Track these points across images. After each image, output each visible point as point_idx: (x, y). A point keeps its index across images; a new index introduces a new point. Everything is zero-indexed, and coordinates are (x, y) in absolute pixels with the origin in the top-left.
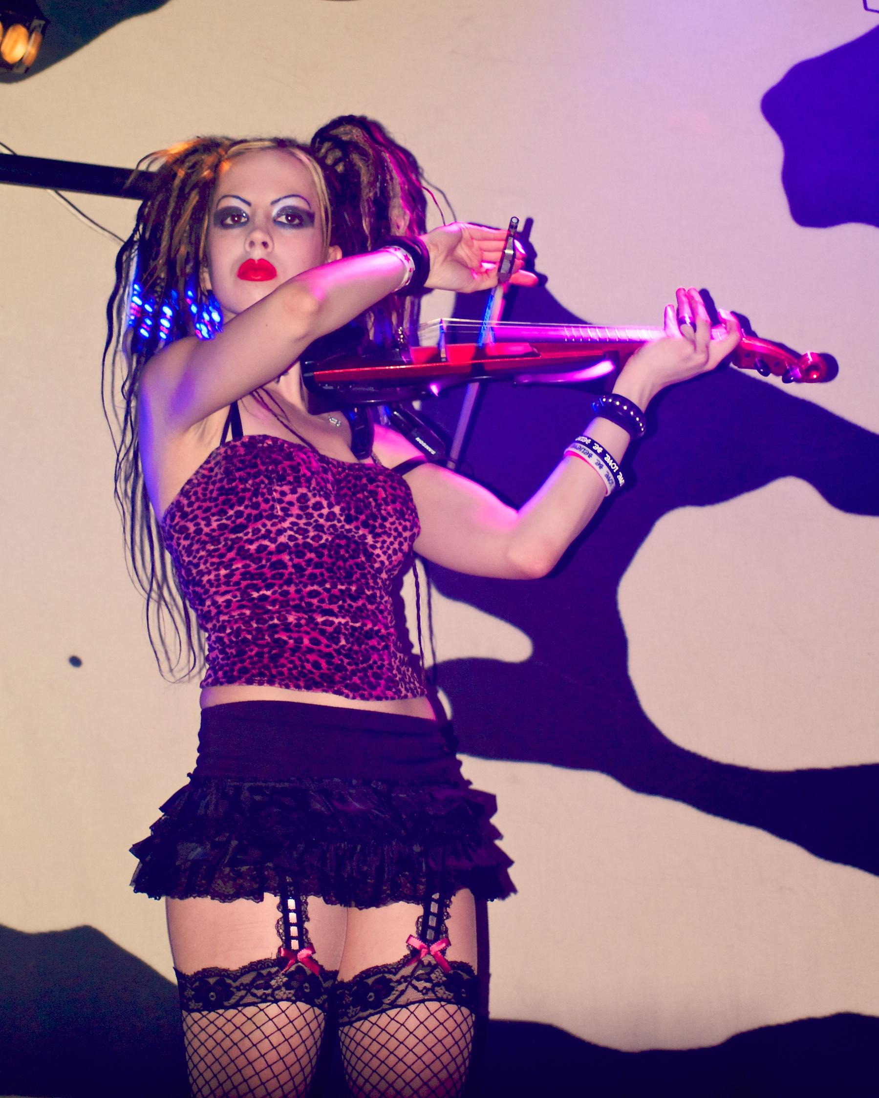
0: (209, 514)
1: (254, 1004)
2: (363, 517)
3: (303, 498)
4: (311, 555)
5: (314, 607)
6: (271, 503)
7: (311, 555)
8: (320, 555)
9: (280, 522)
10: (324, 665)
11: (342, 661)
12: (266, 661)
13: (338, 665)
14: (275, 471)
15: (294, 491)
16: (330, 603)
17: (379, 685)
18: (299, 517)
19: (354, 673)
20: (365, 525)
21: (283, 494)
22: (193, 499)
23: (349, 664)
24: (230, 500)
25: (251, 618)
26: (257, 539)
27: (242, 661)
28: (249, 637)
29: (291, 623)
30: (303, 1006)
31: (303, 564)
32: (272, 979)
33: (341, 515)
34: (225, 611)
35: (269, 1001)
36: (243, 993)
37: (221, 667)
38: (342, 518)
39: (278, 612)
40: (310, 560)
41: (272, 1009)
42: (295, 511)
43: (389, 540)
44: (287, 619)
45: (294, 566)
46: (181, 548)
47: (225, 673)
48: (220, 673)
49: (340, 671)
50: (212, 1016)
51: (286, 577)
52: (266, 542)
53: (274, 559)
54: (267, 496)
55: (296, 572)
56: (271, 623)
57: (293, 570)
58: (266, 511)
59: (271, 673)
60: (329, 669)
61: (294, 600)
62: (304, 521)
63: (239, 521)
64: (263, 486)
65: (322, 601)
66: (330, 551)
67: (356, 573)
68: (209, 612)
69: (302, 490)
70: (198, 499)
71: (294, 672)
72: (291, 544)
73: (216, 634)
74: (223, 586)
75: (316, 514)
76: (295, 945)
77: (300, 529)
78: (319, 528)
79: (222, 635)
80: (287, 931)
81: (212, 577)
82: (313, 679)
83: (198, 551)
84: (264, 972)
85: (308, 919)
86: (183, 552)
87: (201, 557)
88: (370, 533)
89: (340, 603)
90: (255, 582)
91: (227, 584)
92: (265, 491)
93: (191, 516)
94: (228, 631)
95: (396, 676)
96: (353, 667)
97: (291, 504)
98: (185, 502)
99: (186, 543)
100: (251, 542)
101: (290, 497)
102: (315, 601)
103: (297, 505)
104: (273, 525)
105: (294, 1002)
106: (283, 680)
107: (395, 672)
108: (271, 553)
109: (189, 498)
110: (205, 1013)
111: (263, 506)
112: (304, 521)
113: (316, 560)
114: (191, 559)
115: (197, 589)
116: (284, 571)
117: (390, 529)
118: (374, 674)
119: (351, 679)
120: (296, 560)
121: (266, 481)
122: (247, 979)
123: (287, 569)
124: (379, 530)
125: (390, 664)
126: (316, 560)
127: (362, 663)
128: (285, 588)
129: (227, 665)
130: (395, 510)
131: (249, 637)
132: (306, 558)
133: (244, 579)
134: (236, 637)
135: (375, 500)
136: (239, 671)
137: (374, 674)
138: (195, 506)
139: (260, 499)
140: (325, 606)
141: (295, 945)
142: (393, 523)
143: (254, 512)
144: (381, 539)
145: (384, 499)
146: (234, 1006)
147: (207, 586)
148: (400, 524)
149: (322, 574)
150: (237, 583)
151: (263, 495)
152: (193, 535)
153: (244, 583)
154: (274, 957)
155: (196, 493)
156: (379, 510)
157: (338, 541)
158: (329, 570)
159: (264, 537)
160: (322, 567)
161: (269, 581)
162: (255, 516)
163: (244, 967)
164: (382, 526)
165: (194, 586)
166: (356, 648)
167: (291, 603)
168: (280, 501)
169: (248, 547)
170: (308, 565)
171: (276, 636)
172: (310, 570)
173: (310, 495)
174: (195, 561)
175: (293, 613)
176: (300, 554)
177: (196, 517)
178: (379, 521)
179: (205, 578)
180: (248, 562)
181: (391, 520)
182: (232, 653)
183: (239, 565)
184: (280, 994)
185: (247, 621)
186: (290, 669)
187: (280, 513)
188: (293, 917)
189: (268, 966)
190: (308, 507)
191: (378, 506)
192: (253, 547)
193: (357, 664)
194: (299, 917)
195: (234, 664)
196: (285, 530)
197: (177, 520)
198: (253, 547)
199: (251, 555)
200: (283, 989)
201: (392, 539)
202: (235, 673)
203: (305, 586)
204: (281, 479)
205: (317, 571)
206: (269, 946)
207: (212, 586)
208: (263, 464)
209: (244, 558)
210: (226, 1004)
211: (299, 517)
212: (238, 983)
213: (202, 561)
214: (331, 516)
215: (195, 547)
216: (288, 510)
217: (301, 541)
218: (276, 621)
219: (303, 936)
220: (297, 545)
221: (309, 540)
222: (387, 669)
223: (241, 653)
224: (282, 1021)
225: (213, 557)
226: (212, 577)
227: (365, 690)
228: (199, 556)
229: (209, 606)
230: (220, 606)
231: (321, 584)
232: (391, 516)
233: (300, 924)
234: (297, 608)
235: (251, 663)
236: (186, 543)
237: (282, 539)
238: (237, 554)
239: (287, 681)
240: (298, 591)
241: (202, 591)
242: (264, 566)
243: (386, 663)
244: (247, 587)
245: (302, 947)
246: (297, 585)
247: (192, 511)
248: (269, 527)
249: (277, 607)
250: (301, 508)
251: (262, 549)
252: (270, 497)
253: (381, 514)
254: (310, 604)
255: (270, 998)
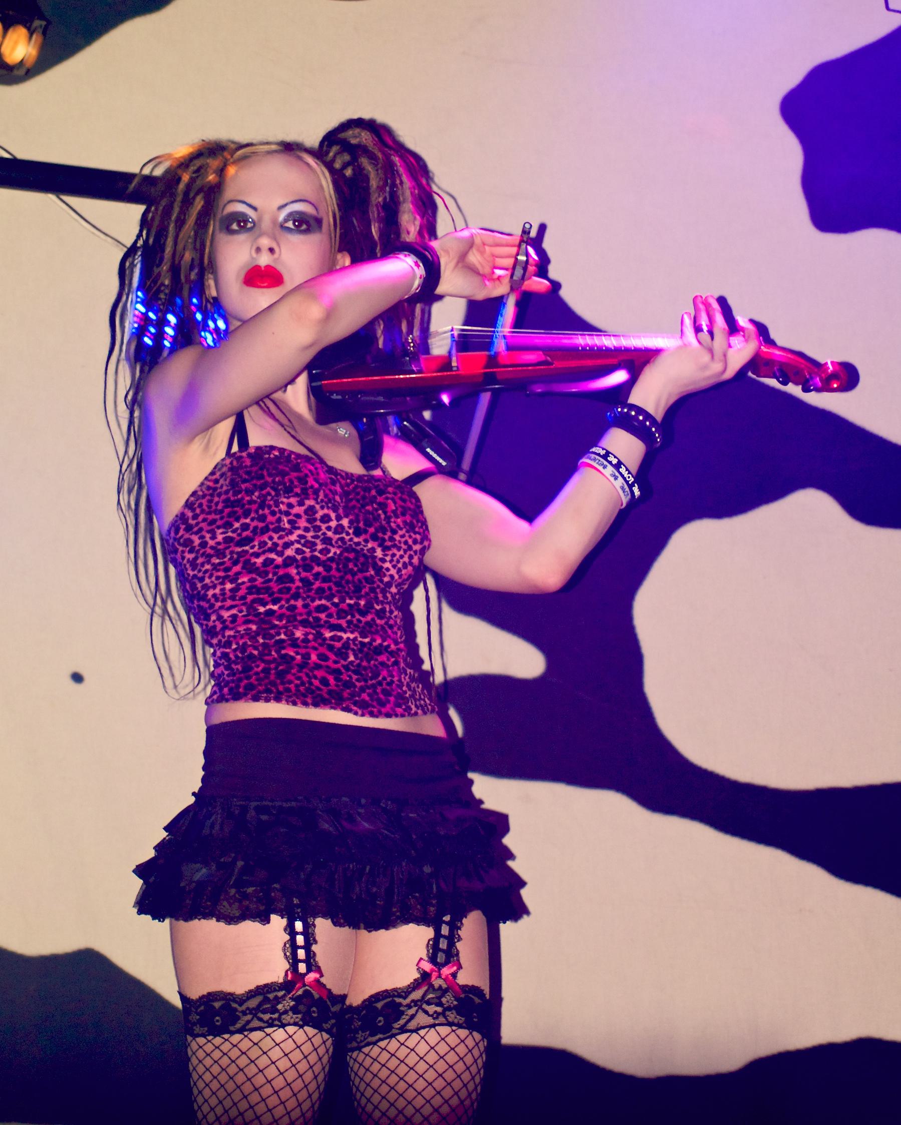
0: (214, 526)
1: (260, 1029)
2: (372, 530)
3: (311, 511)
4: (318, 569)
5: (322, 622)
6: (278, 515)
7: (318, 569)
8: (328, 569)
9: (287, 535)
10: (332, 681)
11: (350, 677)
12: (272, 677)
13: (346, 681)
14: (281, 483)
15: (301, 504)
16: (339, 618)
17: (389, 702)
18: (307, 530)
19: (362, 689)
20: (374, 538)
21: (290, 506)
22: (198, 511)
23: (357, 680)
24: (236, 512)
25: (257, 633)
26: (264, 552)
27: (248, 678)
28: (256, 652)
29: (298, 638)
30: (311, 1031)
31: (311, 578)
32: (279, 1003)
33: (350, 528)
34: (231, 626)
35: (276, 1026)
36: (249, 1017)
37: (227, 684)
38: (351, 531)
39: (285, 627)
40: (318, 574)
41: (279, 1034)
42: (303, 523)
43: (398, 554)
44: (294, 634)
45: (301, 580)
46: (185, 561)
47: (231, 690)
48: (226, 690)
49: (348, 688)
50: (218, 1040)
51: (293, 591)
52: (273, 556)
53: (281, 572)
54: (274, 508)
55: (304, 586)
56: (278, 638)
57: (301, 584)
58: (272, 523)
59: (277, 689)
60: (337, 686)
61: (301, 615)
62: (311, 534)
63: (245, 534)
64: (269, 498)
65: (330, 616)
66: (338, 564)
67: (365, 587)
68: (215, 627)
69: (309, 502)
70: (203, 511)
71: (302, 688)
72: (299, 557)
73: (222, 650)
74: (229, 601)
75: (324, 526)
76: (302, 968)
77: (307, 542)
78: (327, 541)
79: (228, 650)
80: (294, 954)
81: (217, 591)
82: (320, 695)
83: (203, 565)
84: (271, 996)
85: (316, 942)
86: (188, 566)
87: (206, 571)
88: (379, 546)
89: (349, 617)
90: (261, 596)
91: (233, 598)
92: (272, 503)
93: (195, 529)
94: (234, 646)
95: (405, 692)
96: (362, 683)
97: (298, 516)
98: (190, 514)
99: (191, 556)
100: (257, 555)
101: (297, 510)
102: (323, 616)
103: (304, 517)
104: (280, 538)
105: (301, 1027)
106: (290, 697)
107: (404, 688)
108: (277, 567)
109: (193, 510)
110: (210, 1038)
111: (270, 518)
112: (311, 534)
113: (324, 573)
114: (196, 572)
115: (202, 603)
116: (292, 585)
117: (400, 542)
118: (384, 691)
119: (359, 696)
120: (303, 574)
121: (273, 493)
122: (253, 1003)
123: (294, 583)
124: (389, 543)
125: (400, 680)
126: (324, 573)
127: (371, 679)
128: (292, 602)
129: (233, 681)
130: (405, 522)
131: (256, 652)
132: (314, 572)
133: (250, 593)
134: (242, 653)
135: (385, 513)
136: (245, 688)
137: (384, 691)
138: (200, 518)
139: (266, 511)
140: (334, 621)
141: (302, 968)
142: (402, 536)
143: (261, 525)
144: (390, 553)
145: (394, 512)
146: (240, 1031)
147: (213, 600)
148: (410, 537)
149: (330, 589)
150: (243, 598)
151: (269, 507)
152: (197, 548)
153: (250, 598)
154: (281, 980)
155: (201, 505)
156: (389, 522)
157: (346, 554)
158: (338, 584)
159: (271, 550)
160: (330, 581)
161: (275, 596)
162: (262, 529)
163: (250, 991)
164: (392, 539)
165: (199, 601)
166: (365, 663)
167: (299, 618)
168: (287, 514)
169: (254, 560)
170: (316, 579)
171: (283, 652)
172: (317, 584)
173: (318, 507)
174: (200, 575)
175: (301, 628)
176: (308, 568)
177: (201, 530)
178: (389, 534)
179: (210, 593)
180: (254, 576)
181: (401, 533)
182: (237, 669)
183: (245, 579)
184: (287, 1018)
185: (253, 637)
186: (297, 686)
187: (287, 526)
188: (300, 940)
189: (275, 990)
190: (315, 520)
191: (388, 519)
192: (259, 561)
193: (366, 681)
194: (307, 940)
195: (240, 680)
196: (292, 543)
197: (181, 532)
198: (259, 561)
199: (258, 568)
200: (290, 1013)
201: (402, 552)
202: (241, 690)
203: (313, 601)
204: (288, 491)
205: (325, 585)
206: (275, 970)
207: (217, 600)
208: (270, 475)
209: (250, 572)
210: (232, 1028)
211: (307, 530)
212: (244, 1007)
213: (207, 575)
214: (339, 529)
215: (200, 561)
216: (295, 522)
217: (308, 555)
218: (283, 636)
219: (310, 959)
220: (304, 559)
221: (316, 553)
222: (397, 685)
223: (247, 669)
224: (289, 1046)
225: (218, 571)
226: (217, 591)
227: (374, 707)
228: (203, 569)
229: (214, 621)
230: (226, 621)
231: (329, 598)
232: (401, 529)
233: (307, 947)
234: (305, 623)
235: (257, 680)
236: (191, 556)
237: (290, 552)
238: (243, 568)
239: (294, 698)
240: (305, 606)
241: (207, 605)
242: (270, 580)
243: (395, 679)
244: (254, 601)
245: (309, 970)
246: (304, 599)
247: (197, 524)
248: (275, 540)
249: (284, 622)
250: (308, 521)
251: (268, 562)
252: (276, 509)
253: (390, 526)
254: (318, 619)
255: (277, 1023)
